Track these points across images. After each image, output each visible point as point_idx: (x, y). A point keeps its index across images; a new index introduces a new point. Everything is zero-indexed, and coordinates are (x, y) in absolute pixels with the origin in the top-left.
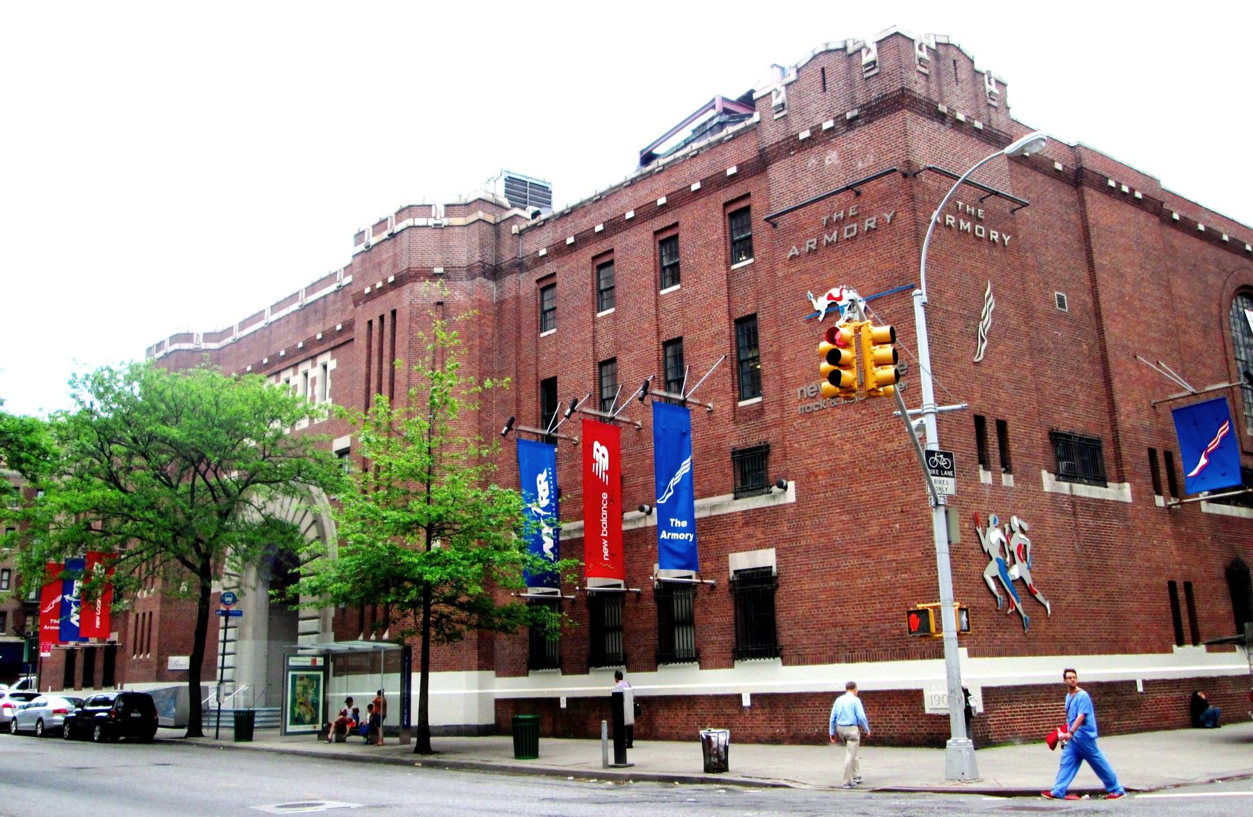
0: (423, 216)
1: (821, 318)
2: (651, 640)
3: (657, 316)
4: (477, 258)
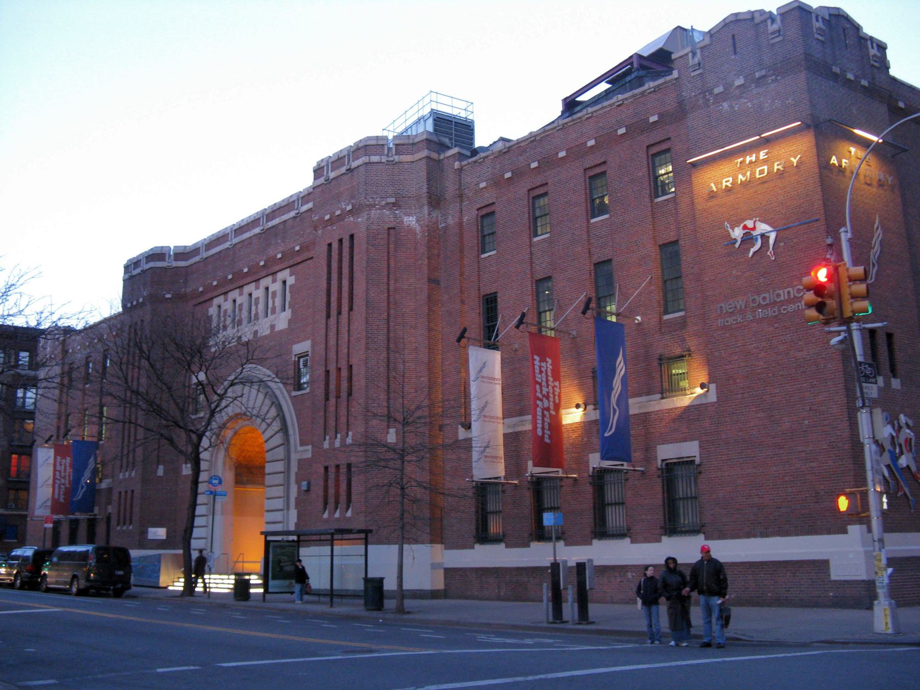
1: (737, 245)
3: (589, 241)
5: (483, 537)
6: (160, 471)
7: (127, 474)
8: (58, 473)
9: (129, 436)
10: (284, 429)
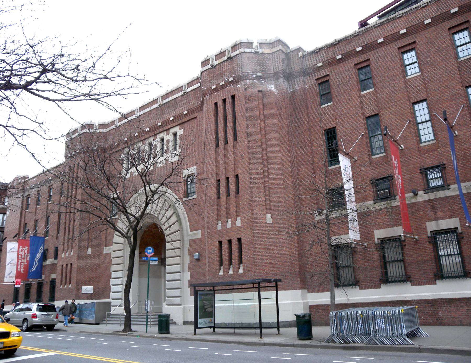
0: (248, 48)
2: (378, 272)
4: (281, 68)
5: (386, 280)
6: (89, 251)
7: (67, 254)
8: (20, 256)
9: (69, 231)
10: (179, 221)
